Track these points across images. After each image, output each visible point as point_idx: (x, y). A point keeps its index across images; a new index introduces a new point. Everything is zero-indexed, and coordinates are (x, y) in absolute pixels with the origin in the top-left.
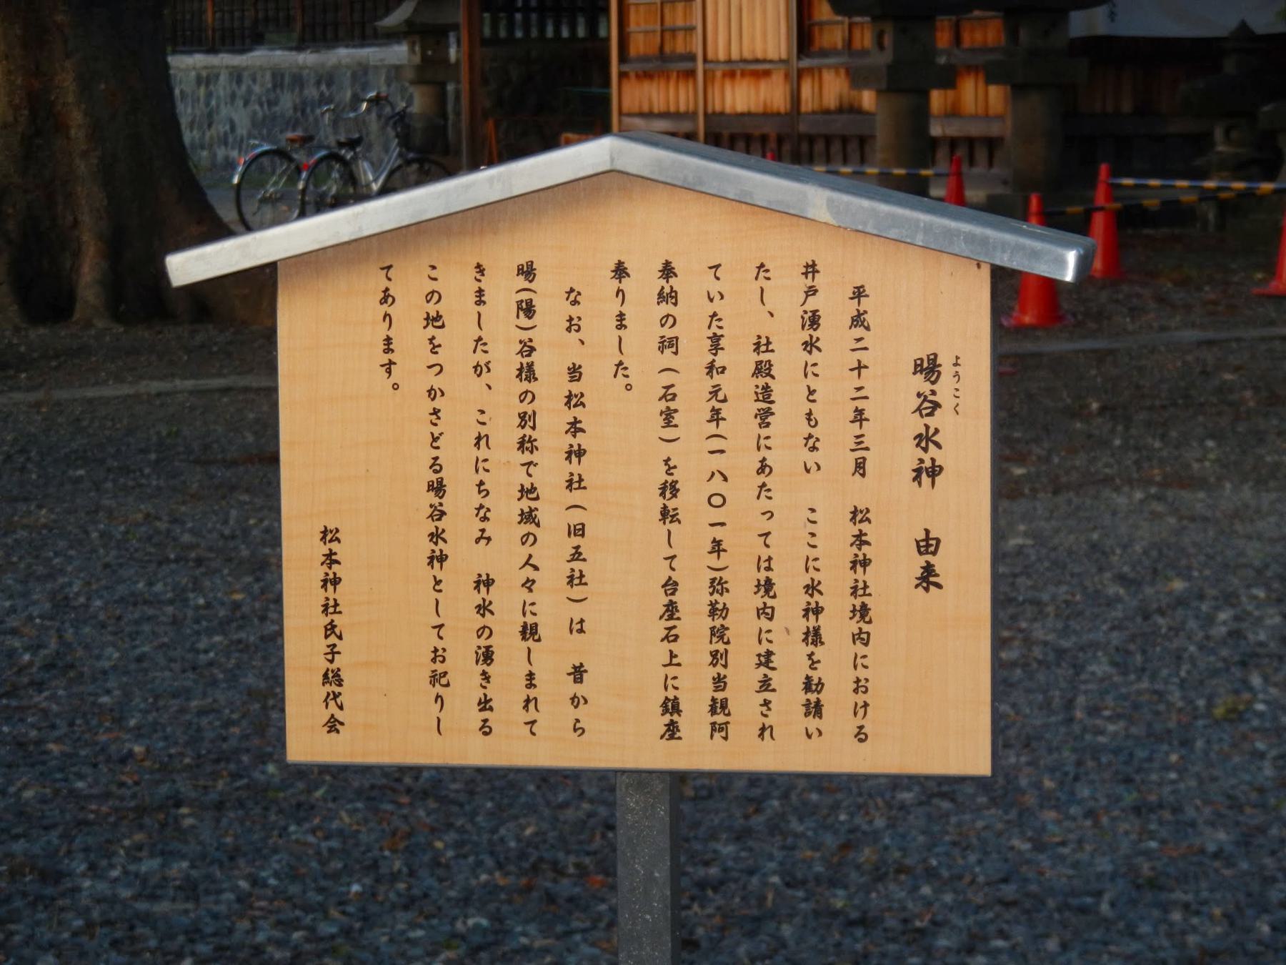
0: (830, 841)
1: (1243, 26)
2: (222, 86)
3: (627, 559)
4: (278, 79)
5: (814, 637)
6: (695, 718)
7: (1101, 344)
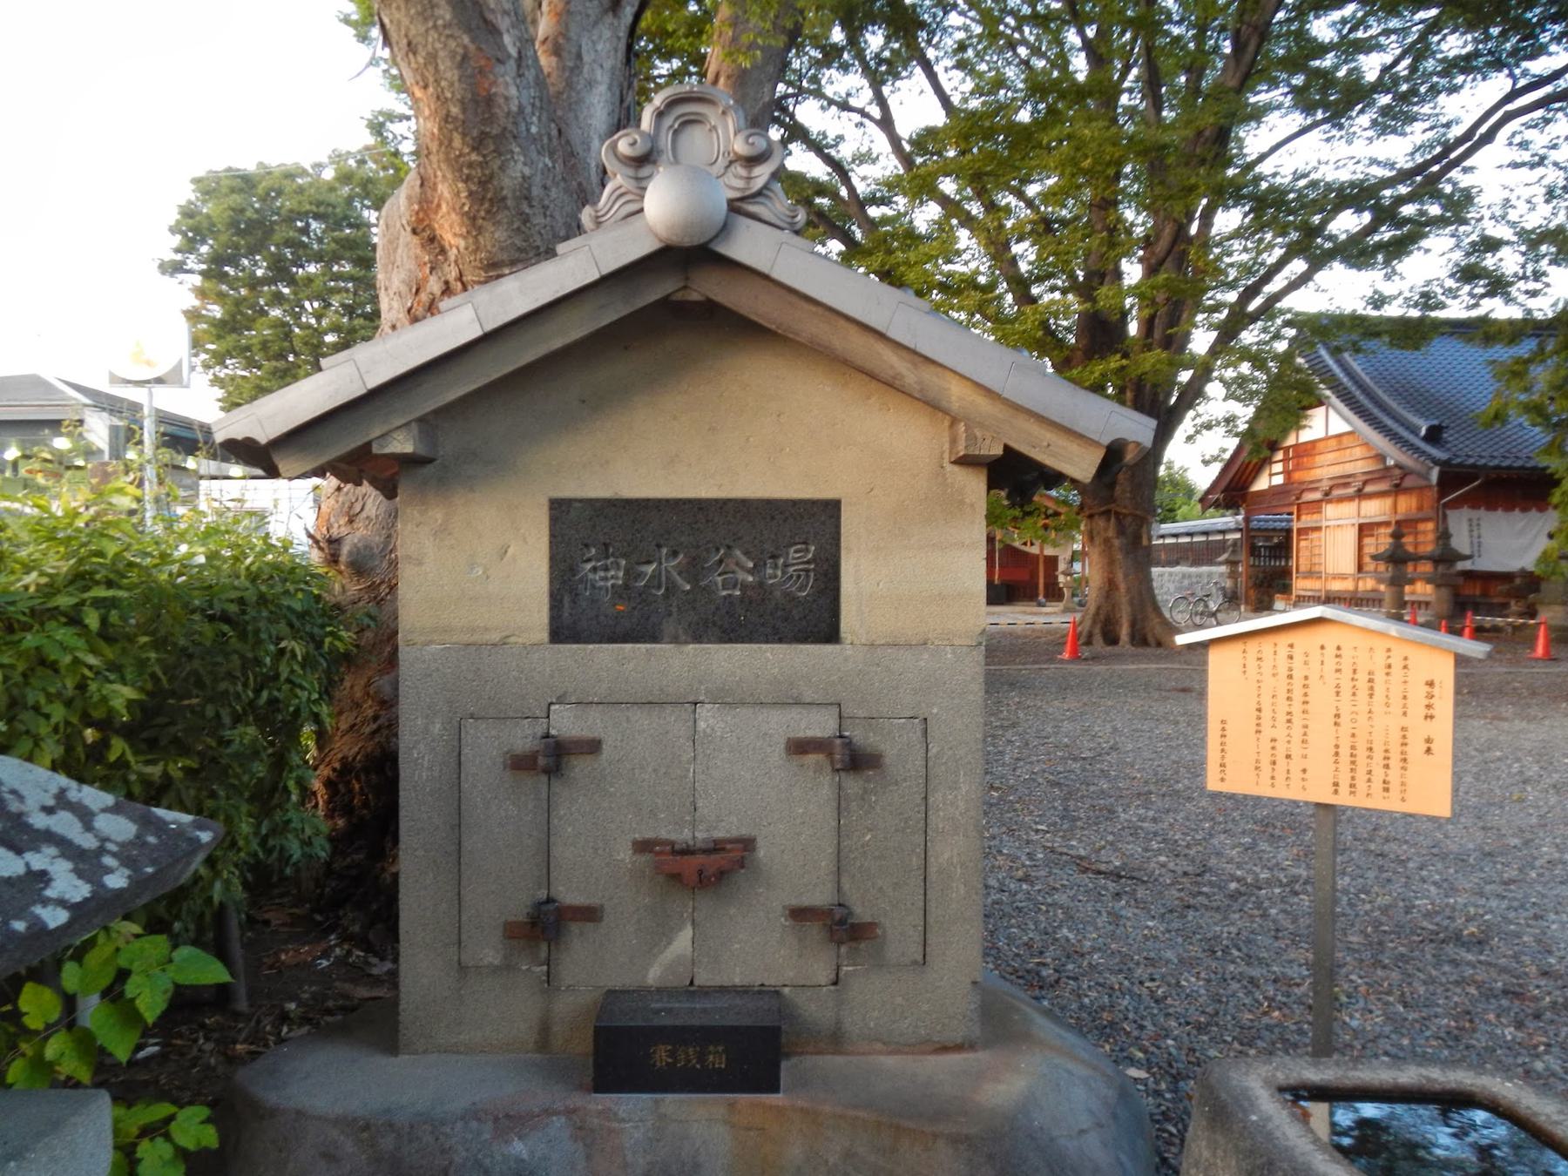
0: (1370, 827)
2: (1166, 577)
3: (1322, 736)
4: (1184, 576)
5: (1387, 766)
6: (1344, 788)
7: (1468, 671)
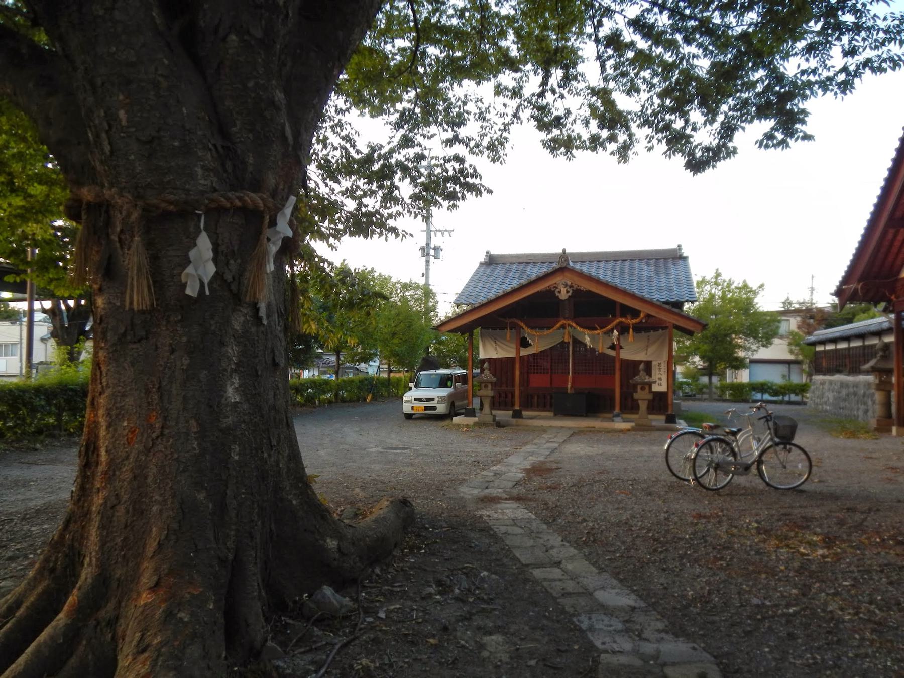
1: (478, 84)
2: (826, 386)
